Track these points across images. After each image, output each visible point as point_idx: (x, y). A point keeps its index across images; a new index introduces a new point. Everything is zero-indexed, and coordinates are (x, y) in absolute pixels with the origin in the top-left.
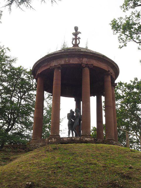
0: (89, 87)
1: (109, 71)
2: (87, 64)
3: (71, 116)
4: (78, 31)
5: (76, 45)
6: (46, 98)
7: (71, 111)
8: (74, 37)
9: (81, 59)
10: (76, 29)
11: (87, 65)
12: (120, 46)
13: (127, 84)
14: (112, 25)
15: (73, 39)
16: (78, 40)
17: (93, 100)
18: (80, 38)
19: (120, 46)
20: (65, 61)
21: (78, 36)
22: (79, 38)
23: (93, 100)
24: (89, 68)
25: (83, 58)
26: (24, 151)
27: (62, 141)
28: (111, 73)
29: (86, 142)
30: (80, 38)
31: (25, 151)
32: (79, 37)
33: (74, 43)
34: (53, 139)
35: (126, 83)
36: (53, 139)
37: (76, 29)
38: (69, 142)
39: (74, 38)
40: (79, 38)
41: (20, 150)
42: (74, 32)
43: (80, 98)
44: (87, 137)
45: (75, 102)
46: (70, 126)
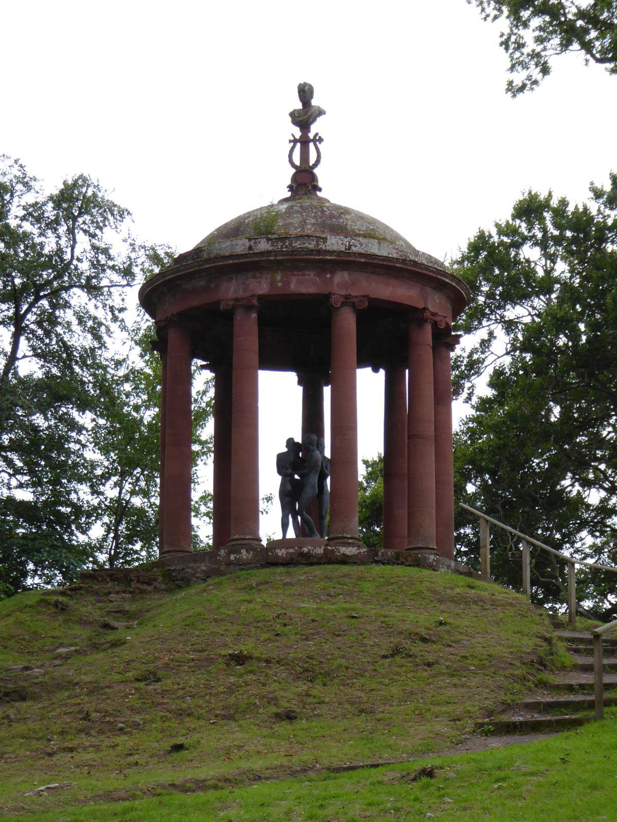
0: (355, 349)
1: (425, 309)
2: (347, 297)
3: (285, 464)
4: (314, 102)
5: (304, 181)
6: (99, 258)
7: (320, 190)
8: (297, 133)
9: (328, 276)
10: (305, 93)
11: (348, 301)
12: (510, 83)
13: (571, 209)
14: (370, 469)
15: (295, 141)
16: (311, 145)
17: (370, 385)
18: (321, 140)
19: (510, 83)
20: (273, 283)
21: (314, 129)
22: (318, 140)
23: (370, 385)
24: (353, 305)
25: (332, 273)
26: (149, 588)
27: (269, 557)
28: (434, 314)
29: (345, 560)
30: (321, 140)
31: (155, 587)
32: (317, 134)
33: (297, 160)
34: (244, 551)
35: (564, 203)
36: (244, 551)
37: (305, 93)
38: (292, 559)
39: (298, 137)
40: (318, 140)
41: (140, 586)
42: (299, 106)
43: (318, 371)
44: (349, 545)
45: (301, 389)
46: (288, 499)
